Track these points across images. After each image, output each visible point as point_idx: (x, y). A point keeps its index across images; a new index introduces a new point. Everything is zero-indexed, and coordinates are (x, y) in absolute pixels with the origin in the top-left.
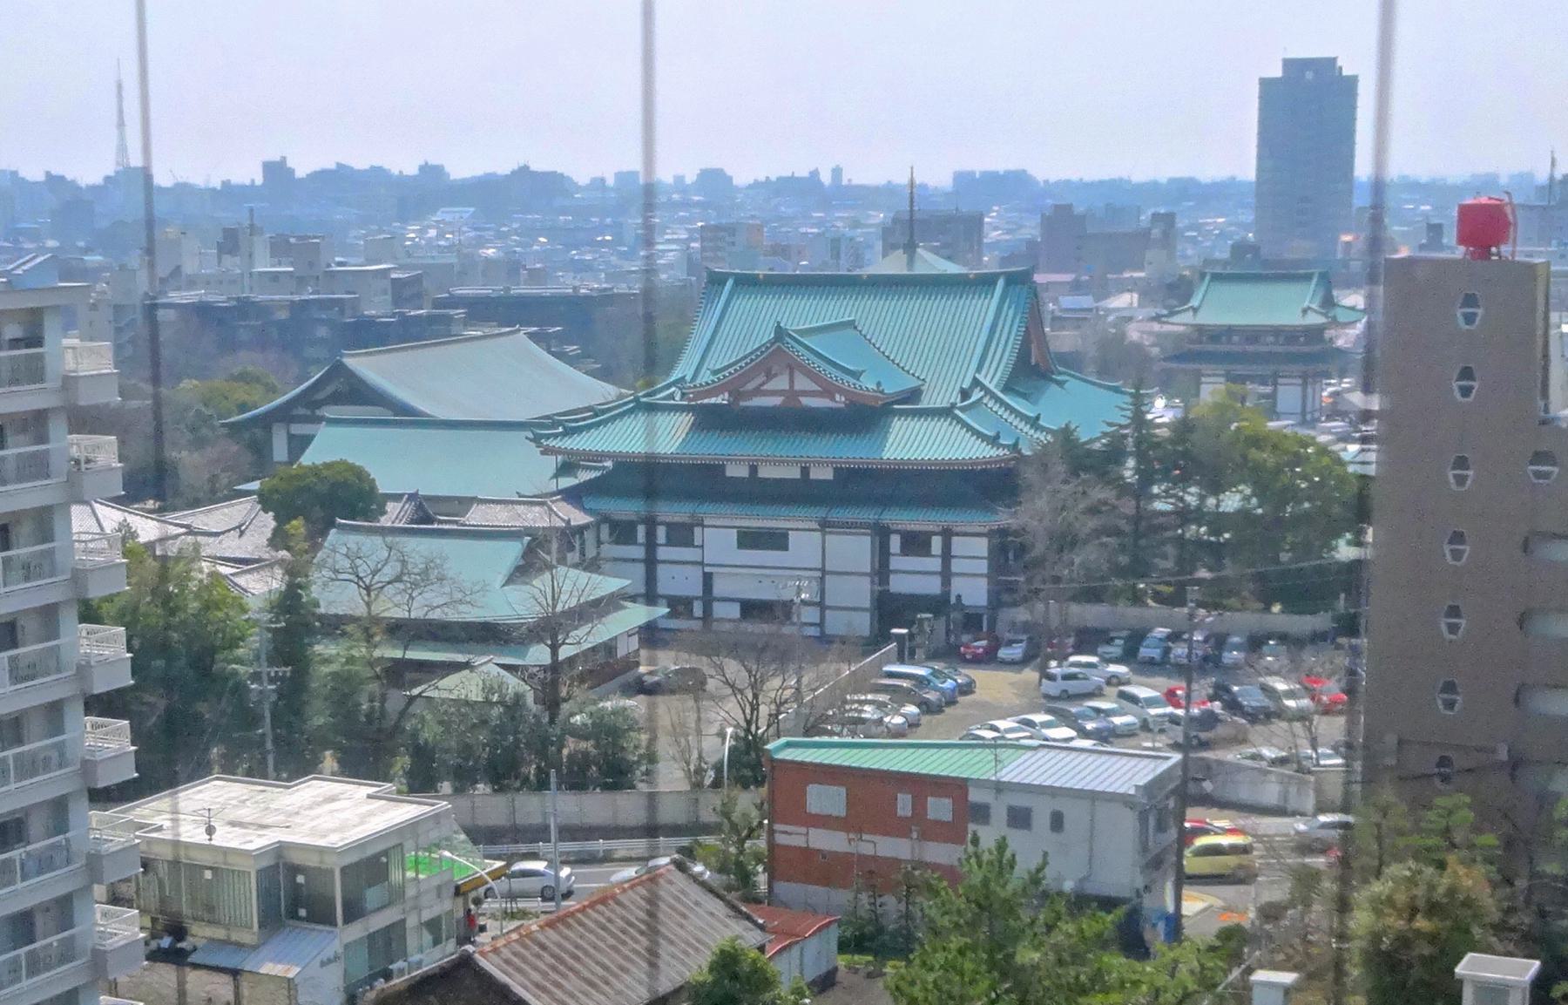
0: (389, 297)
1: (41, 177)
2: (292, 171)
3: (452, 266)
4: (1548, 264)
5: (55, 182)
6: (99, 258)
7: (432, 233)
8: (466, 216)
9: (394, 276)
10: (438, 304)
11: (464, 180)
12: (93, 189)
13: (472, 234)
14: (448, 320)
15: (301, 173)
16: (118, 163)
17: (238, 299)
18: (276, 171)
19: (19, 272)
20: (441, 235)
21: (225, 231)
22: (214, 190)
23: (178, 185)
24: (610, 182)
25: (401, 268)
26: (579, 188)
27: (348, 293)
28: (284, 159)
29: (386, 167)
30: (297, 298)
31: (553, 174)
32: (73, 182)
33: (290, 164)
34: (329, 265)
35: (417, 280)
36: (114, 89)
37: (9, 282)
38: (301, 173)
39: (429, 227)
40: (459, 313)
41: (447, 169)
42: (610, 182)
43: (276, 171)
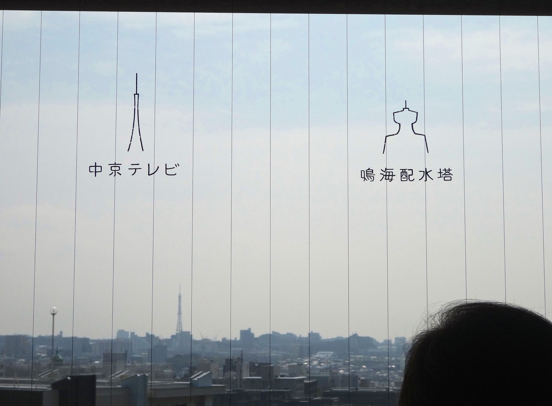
0: (303, 391)
1: (144, 335)
2: (253, 335)
3: (328, 377)
4: (145, 378)
5: (151, 337)
6: (170, 371)
7: (315, 363)
8: (329, 355)
9: (305, 382)
10: (325, 395)
11: (328, 340)
12: (167, 340)
13: (333, 363)
14: (331, 402)
15: (257, 335)
16: (177, 330)
17: (238, 391)
18: (246, 334)
19: (196, 379)
20: (320, 363)
21: (227, 360)
22: (219, 342)
23: (203, 340)
24: (393, 342)
25: (309, 378)
26: (379, 344)
27: (286, 389)
28: (250, 330)
29: (294, 333)
30: (263, 391)
31: (371, 338)
32: (158, 337)
33: (252, 331)
34: (277, 376)
35: (315, 384)
36: (178, 299)
37: (191, 384)
38: (257, 335)
39: (314, 360)
40: (335, 399)
41: (321, 335)
42: (393, 342)
43: (246, 334)
